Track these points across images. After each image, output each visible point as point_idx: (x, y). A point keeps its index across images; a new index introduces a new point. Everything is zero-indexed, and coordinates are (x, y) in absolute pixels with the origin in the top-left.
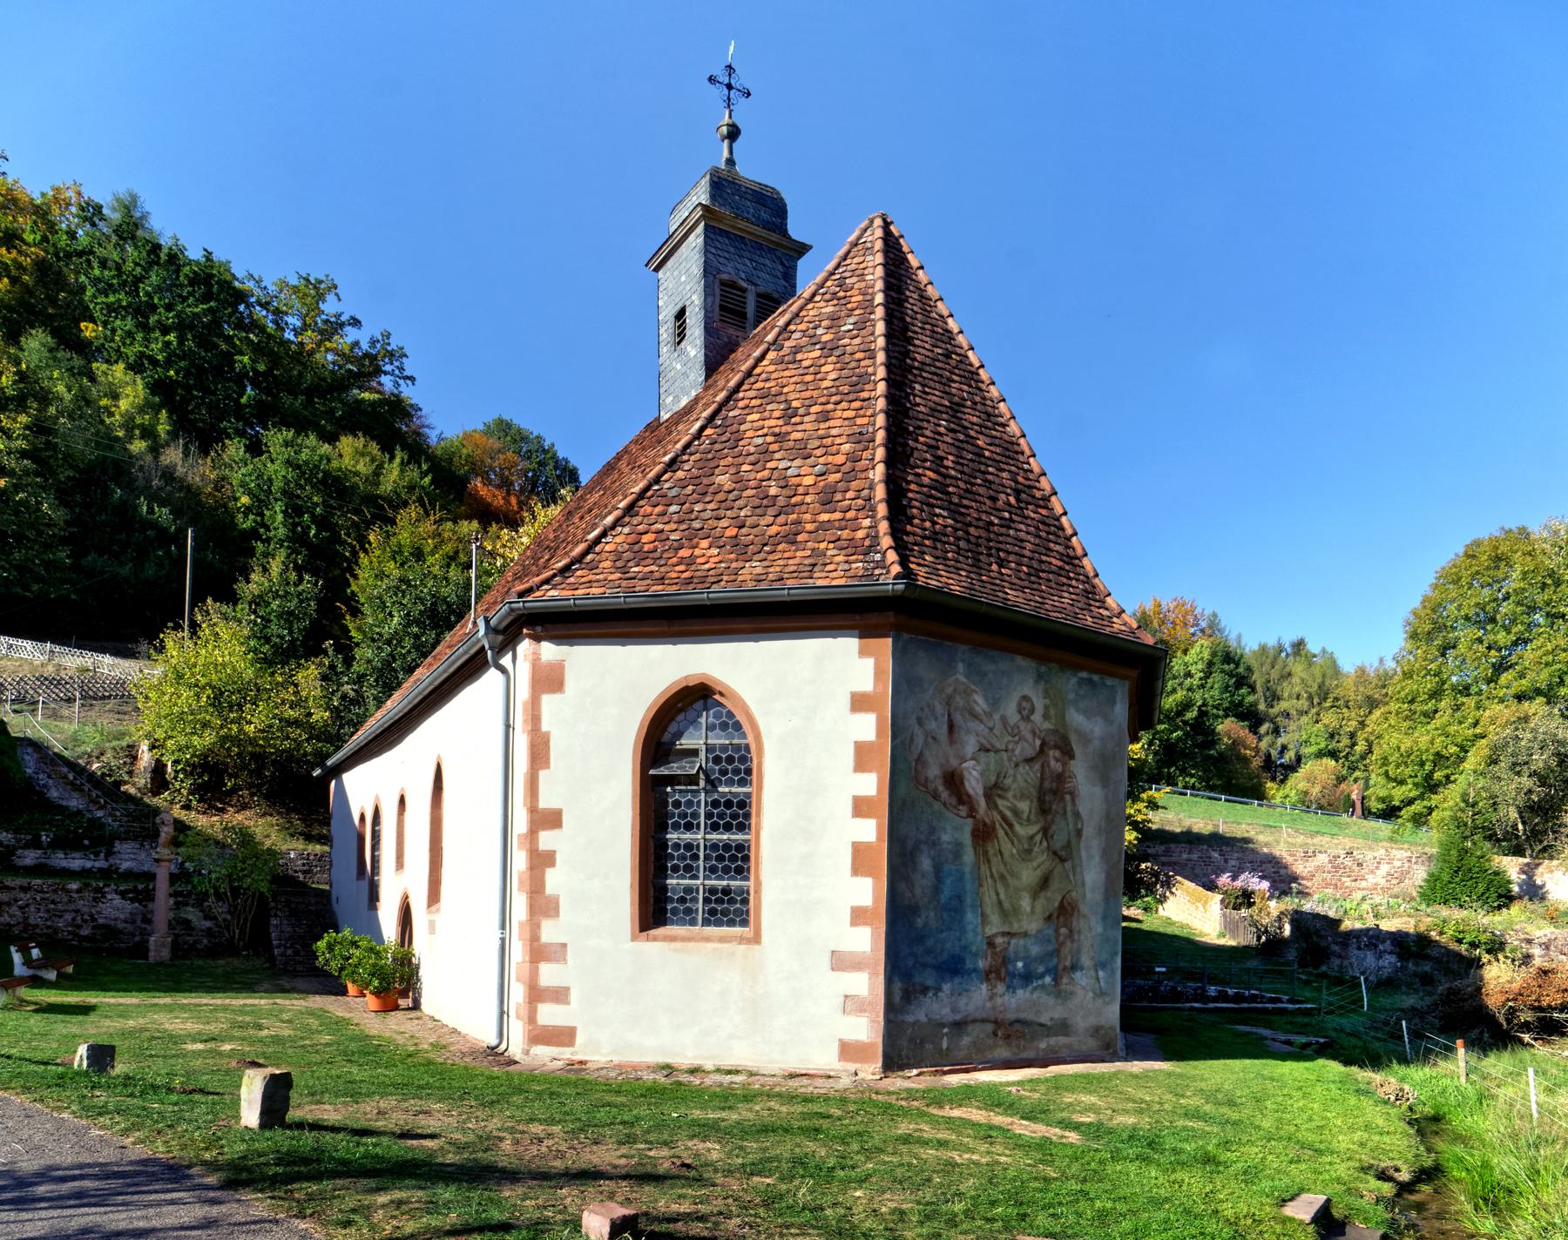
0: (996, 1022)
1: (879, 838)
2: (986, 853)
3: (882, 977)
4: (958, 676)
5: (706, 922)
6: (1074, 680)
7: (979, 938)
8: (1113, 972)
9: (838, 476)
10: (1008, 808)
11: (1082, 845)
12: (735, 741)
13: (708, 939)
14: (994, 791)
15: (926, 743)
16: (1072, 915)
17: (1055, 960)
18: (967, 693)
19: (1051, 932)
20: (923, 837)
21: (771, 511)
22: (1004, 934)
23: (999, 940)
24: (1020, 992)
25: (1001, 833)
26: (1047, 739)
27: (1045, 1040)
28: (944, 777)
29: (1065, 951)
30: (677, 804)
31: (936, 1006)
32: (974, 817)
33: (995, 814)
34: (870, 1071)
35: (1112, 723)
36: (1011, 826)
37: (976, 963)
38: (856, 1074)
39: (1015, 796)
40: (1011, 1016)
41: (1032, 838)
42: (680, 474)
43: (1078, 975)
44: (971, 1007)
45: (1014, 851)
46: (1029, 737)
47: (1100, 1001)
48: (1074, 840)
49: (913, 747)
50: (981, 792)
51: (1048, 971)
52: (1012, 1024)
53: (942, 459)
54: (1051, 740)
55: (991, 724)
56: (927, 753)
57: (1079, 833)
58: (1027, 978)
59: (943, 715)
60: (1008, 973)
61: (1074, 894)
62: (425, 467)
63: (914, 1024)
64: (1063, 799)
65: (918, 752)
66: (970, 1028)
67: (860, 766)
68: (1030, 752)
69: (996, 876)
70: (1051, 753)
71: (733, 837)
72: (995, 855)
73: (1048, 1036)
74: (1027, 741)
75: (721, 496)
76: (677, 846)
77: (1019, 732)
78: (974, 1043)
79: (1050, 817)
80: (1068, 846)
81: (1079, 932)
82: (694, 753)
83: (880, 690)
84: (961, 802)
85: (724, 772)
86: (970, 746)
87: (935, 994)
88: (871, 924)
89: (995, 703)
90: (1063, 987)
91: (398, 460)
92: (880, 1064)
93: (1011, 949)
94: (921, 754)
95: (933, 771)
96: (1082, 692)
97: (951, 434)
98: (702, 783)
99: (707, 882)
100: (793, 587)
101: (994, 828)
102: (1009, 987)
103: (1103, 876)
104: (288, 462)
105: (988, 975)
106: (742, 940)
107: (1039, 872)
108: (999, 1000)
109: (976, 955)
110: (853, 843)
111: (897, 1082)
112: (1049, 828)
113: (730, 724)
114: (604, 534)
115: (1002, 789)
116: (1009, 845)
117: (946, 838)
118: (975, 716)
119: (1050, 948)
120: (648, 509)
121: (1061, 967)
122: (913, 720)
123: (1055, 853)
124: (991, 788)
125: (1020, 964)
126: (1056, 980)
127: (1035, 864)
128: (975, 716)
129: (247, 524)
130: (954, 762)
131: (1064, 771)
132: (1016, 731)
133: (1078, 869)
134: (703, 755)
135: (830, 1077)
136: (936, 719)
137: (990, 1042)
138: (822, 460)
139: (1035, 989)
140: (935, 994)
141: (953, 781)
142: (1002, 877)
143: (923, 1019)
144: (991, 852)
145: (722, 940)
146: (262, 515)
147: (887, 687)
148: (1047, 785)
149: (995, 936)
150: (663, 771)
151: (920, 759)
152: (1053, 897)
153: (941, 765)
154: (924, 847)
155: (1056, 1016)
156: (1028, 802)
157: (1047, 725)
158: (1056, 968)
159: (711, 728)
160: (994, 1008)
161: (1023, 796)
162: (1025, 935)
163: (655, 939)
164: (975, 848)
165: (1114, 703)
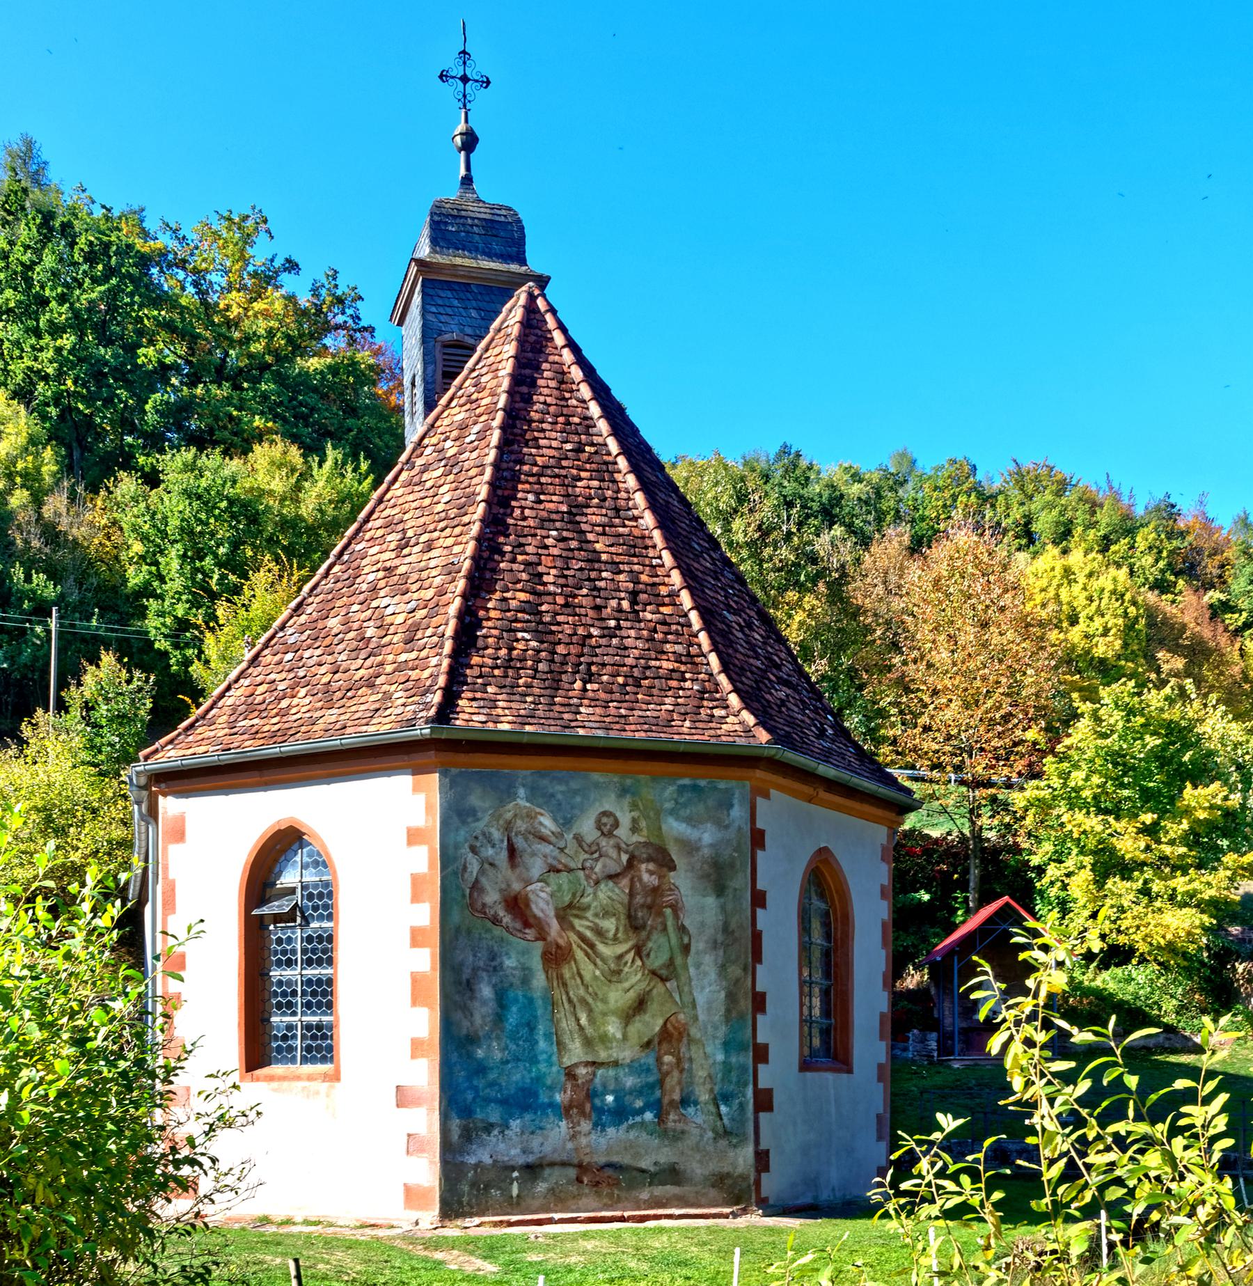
0: (580, 1166)
1: (433, 968)
2: (560, 977)
3: (437, 1112)
4: (519, 801)
5: (304, 1060)
6: (671, 790)
9: (424, 612)
10: (588, 927)
12: (324, 878)
13: (298, 1078)
14: (566, 913)
15: (482, 871)
17: (658, 1093)
18: (531, 816)
19: (651, 1060)
20: (481, 964)
21: (363, 654)
22: (587, 1064)
23: (582, 1071)
24: (611, 1131)
25: (579, 955)
26: (637, 853)
27: (647, 1189)
28: (506, 901)
29: (672, 1081)
30: (279, 941)
32: (544, 939)
34: (429, 1216)
36: (592, 946)
37: (551, 1097)
38: (417, 1223)
40: (602, 1160)
41: (620, 957)
42: (303, 618)
43: (691, 1110)
44: (547, 1149)
45: (598, 973)
47: (723, 1143)
49: (466, 876)
50: (552, 913)
52: (602, 1168)
53: (541, 575)
55: (562, 845)
56: (484, 881)
58: (620, 1113)
60: (593, 1107)
62: (364, 466)
63: (478, 1165)
64: (660, 914)
66: (547, 1171)
67: (416, 898)
68: (614, 868)
70: (643, 866)
71: (284, 973)
72: (573, 978)
73: (651, 1184)
75: (327, 641)
76: (280, 983)
77: (599, 849)
78: (553, 1189)
79: (644, 934)
82: (292, 891)
83: (430, 824)
84: (527, 925)
85: (315, 908)
86: (537, 868)
87: (502, 1132)
88: (427, 1057)
89: (566, 823)
90: (670, 1125)
91: (329, 464)
92: (437, 1211)
93: (597, 1080)
94: (477, 881)
95: (492, 897)
96: (682, 800)
97: (561, 545)
98: (299, 920)
99: (304, 1019)
100: (351, 738)
101: (571, 950)
102: (595, 1125)
104: (188, 494)
105: (566, 1111)
106: (326, 1078)
108: (584, 1141)
109: (551, 1088)
111: (452, 1231)
112: (644, 945)
113: (321, 863)
114: (228, 688)
115: (579, 909)
116: (591, 967)
117: (510, 962)
118: (543, 839)
119: (651, 1079)
120: (269, 657)
121: (666, 1100)
122: (465, 850)
124: (564, 909)
126: (661, 1117)
127: (627, 985)
128: (543, 839)
129: (135, 577)
130: (516, 886)
132: (594, 848)
134: (299, 891)
135: (392, 1227)
136: (493, 846)
137: (573, 1189)
138: (415, 596)
139: (631, 1127)
141: (517, 905)
143: (487, 1160)
144: (567, 975)
145: (310, 1078)
146: (157, 564)
147: (435, 821)
149: (576, 1065)
150: (265, 910)
151: (476, 886)
152: (652, 1023)
154: (484, 974)
155: (662, 1160)
156: (613, 920)
157: (636, 838)
158: (659, 1102)
159: (304, 867)
160: (576, 1149)
161: (606, 914)
163: (258, 1080)
164: (547, 972)
165: (731, 806)
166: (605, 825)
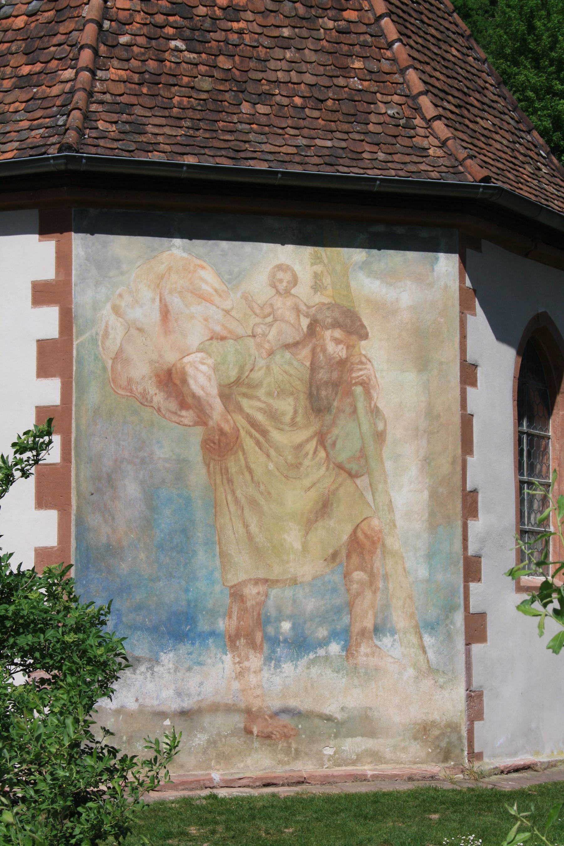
0: (248, 712)
2: (225, 472)
7: (218, 588)
8: (449, 637)
10: (260, 409)
11: (386, 453)
16: (372, 553)
17: (346, 620)
19: (337, 578)
22: (257, 582)
23: (251, 591)
24: (287, 667)
25: (248, 443)
26: (320, 317)
31: (150, 686)
32: (205, 424)
36: (264, 433)
40: (276, 704)
41: (300, 447)
43: (387, 641)
45: (271, 466)
46: (291, 316)
48: (371, 448)
49: (108, 343)
50: (214, 391)
51: (334, 635)
52: (276, 714)
54: (327, 317)
55: (227, 305)
57: (380, 437)
61: (375, 522)
64: (349, 393)
66: (207, 720)
68: (292, 336)
69: (243, 500)
70: (328, 334)
73: (336, 736)
79: (328, 418)
80: (362, 454)
81: (386, 577)
83: (61, 278)
84: (183, 405)
90: (362, 659)
93: (270, 603)
102: (269, 659)
107: (313, 494)
108: (253, 679)
110: (38, 341)
118: (203, 298)
119: (338, 601)
121: (356, 628)
125: (286, 626)
128: (203, 298)
130: (171, 357)
132: (267, 310)
133: (380, 487)
139: (313, 662)
140: (151, 668)
142: (253, 502)
143: (132, 706)
144: (233, 469)
148: (322, 375)
153: (151, 362)
156: (291, 400)
157: (318, 298)
158: (347, 631)
161: (282, 393)
162: (294, 582)
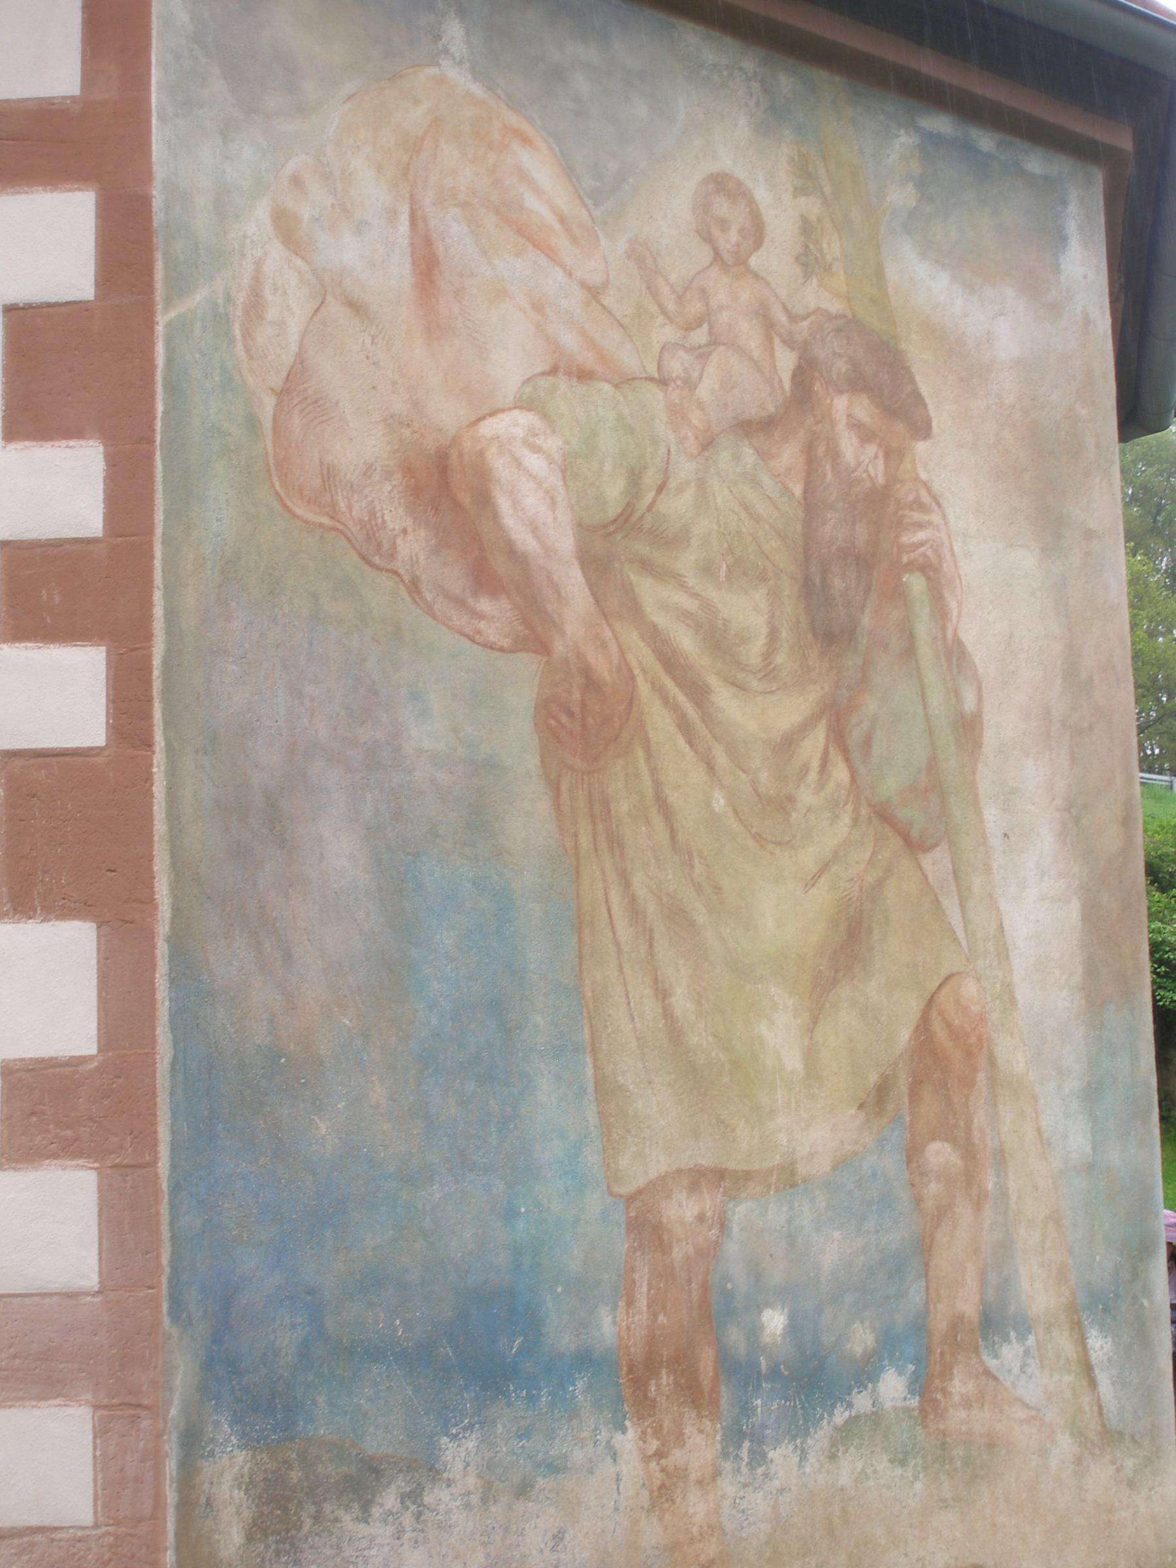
7: (594, 1202)
8: (1142, 1335)
10: (684, 616)
11: (985, 780)
19: (891, 1164)
24: (781, 1456)
26: (820, 352)
32: (542, 647)
33: (632, 637)
35: (1055, 309)
36: (699, 693)
39: (707, 569)
41: (787, 744)
43: (1010, 1353)
45: (719, 802)
46: (750, 335)
47: (1100, 1474)
49: (263, 335)
50: (566, 543)
55: (592, 270)
59: (392, 215)
60: (728, 1366)
64: (898, 594)
65: (288, 359)
70: (841, 404)
74: (743, 352)
79: (852, 662)
81: (1001, 1158)
90: (956, 1418)
102: (735, 1435)
103: (1074, 912)
107: (822, 895)
108: (697, 1506)
110: (10, 309)
116: (697, 775)
123: (884, 814)
125: (775, 1321)
131: (892, 480)
132: (695, 308)
139: (845, 1435)
140: (413, 1496)
142: (677, 915)
148: (832, 529)
149: (660, 1186)
153: (392, 422)
156: (759, 595)
158: (920, 1326)
164: (555, 787)
166: (724, 224)
